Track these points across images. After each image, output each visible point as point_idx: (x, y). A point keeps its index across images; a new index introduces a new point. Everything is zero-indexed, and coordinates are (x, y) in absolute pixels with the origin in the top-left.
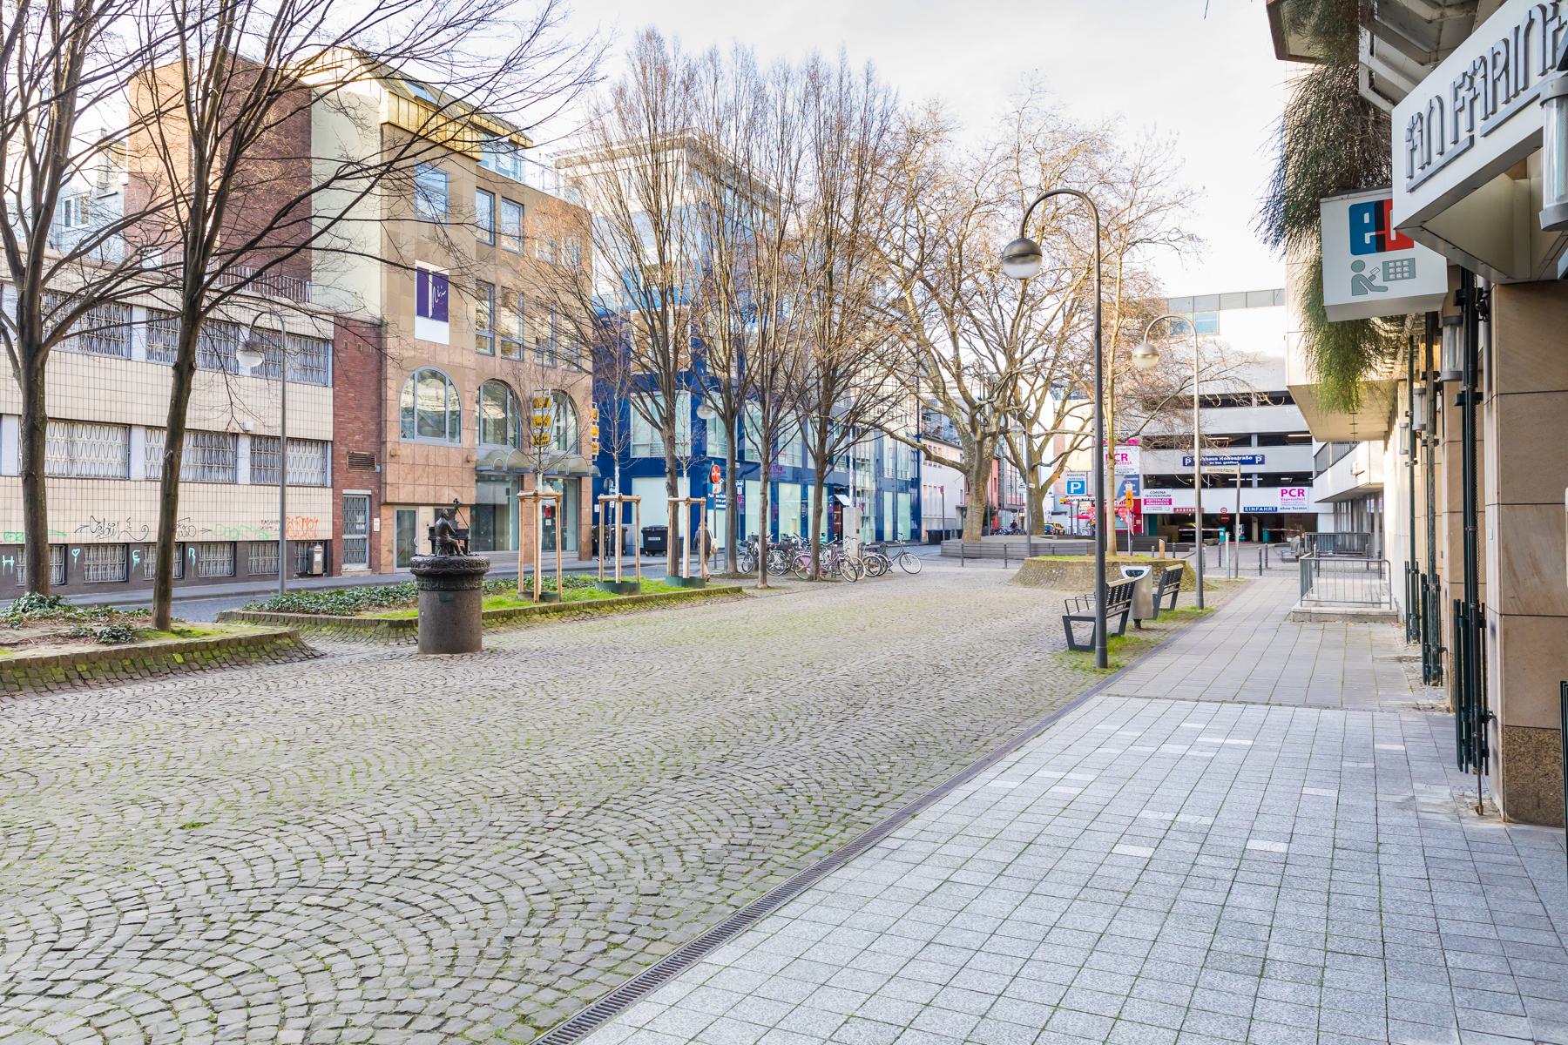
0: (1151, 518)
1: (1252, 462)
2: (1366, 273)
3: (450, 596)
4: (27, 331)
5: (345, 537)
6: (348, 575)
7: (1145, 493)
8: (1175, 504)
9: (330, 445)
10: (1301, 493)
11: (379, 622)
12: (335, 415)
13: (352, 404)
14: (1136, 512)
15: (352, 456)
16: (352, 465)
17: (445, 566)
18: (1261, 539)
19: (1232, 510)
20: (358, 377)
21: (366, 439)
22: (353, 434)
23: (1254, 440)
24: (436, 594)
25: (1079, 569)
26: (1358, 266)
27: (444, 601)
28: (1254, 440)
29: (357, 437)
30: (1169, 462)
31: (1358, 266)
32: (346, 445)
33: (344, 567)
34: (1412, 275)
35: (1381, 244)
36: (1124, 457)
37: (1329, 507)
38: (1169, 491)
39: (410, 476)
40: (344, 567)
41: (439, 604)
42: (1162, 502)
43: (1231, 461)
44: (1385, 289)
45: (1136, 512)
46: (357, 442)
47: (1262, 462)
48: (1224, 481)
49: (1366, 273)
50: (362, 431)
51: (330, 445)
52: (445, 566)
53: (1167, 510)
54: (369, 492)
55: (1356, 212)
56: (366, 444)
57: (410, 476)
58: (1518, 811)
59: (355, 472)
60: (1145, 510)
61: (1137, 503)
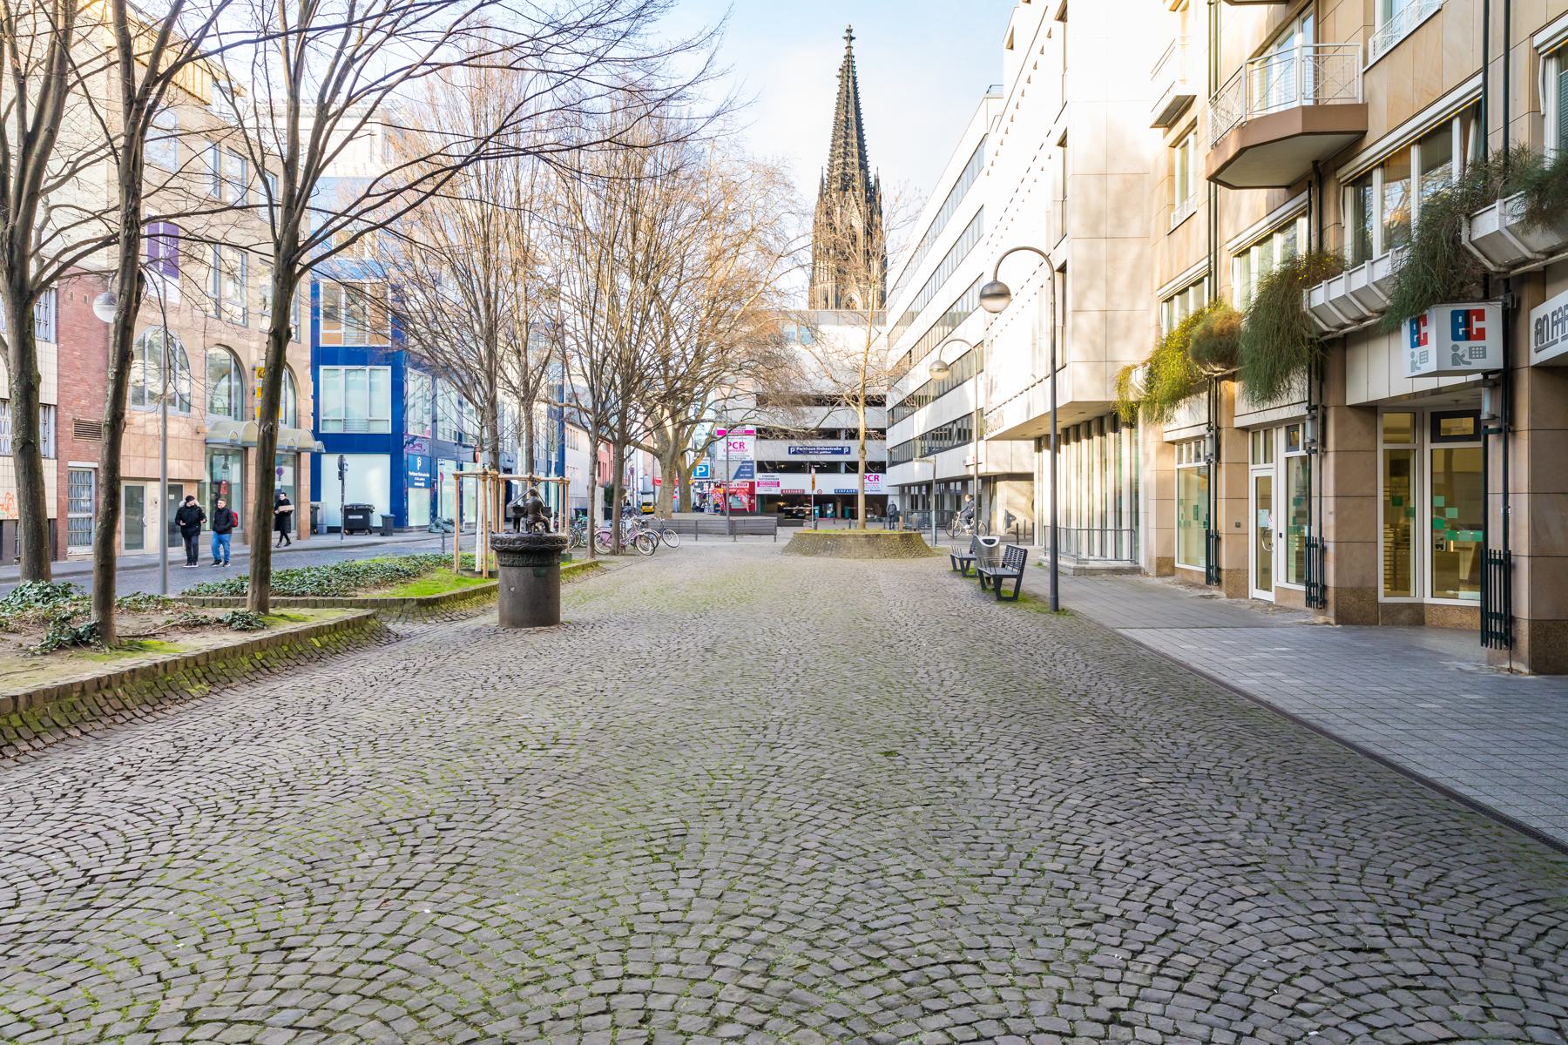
0: (761, 496)
1: (841, 452)
2: (1460, 352)
3: (543, 571)
4: (17, 273)
5: (70, 515)
6: (74, 560)
7: (758, 477)
8: (783, 486)
9: (52, 409)
10: (876, 478)
11: (404, 601)
12: (59, 376)
13: (78, 363)
14: (751, 493)
15: (78, 423)
16: (78, 434)
17: (542, 543)
18: (843, 516)
19: (808, 491)
20: (85, 334)
21: (92, 405)
22: (79, 398)
23: (843, 434)
24: (530, 570)
25: (851, 540)
26: (1455, 348)
27: (537, 576)
28: (843, 434)
29: (83, 402)
30: (777, 451)
31: (1455, 348)
32: (72, 411)
33: (70, 549)
34: (1485, 357)
35: (1468, 336)
36: (741, 445)
37: (897, 491)
38: (777, 475)
39: (140, 448)
40: (70, 549)
41: (533, 579)
42: (772, 484)
43: (823, 451)
44: (1470, 363)
45: (751, 493)
46: (83, 407)
47: (848, 453)
48: (832, 468)
49: (1460, 352)
50: (88, 395)
51: (52, 409)
52: (542, 543)
53: (775, 491)
54: (96, 465)
55: (1455, 314)
56: (92, 410)
57: (140, 448)
58: (1536, 669)
59: (81, 443)
60: (758, 491)
61: (752, 484)
